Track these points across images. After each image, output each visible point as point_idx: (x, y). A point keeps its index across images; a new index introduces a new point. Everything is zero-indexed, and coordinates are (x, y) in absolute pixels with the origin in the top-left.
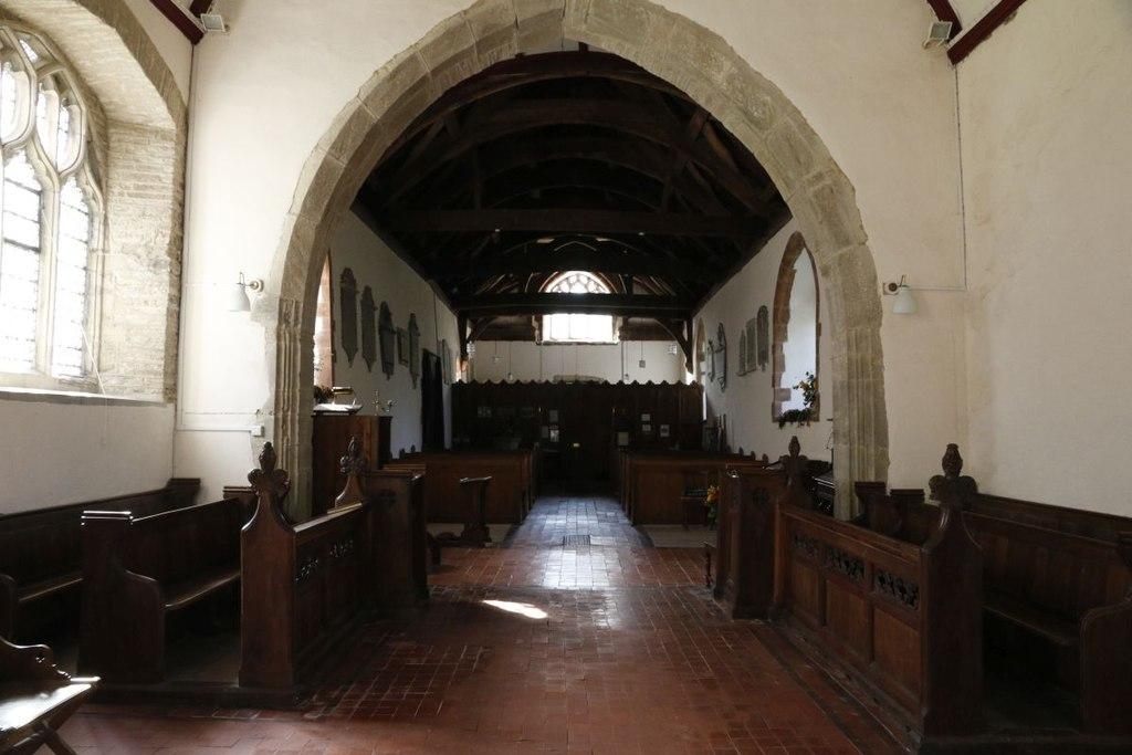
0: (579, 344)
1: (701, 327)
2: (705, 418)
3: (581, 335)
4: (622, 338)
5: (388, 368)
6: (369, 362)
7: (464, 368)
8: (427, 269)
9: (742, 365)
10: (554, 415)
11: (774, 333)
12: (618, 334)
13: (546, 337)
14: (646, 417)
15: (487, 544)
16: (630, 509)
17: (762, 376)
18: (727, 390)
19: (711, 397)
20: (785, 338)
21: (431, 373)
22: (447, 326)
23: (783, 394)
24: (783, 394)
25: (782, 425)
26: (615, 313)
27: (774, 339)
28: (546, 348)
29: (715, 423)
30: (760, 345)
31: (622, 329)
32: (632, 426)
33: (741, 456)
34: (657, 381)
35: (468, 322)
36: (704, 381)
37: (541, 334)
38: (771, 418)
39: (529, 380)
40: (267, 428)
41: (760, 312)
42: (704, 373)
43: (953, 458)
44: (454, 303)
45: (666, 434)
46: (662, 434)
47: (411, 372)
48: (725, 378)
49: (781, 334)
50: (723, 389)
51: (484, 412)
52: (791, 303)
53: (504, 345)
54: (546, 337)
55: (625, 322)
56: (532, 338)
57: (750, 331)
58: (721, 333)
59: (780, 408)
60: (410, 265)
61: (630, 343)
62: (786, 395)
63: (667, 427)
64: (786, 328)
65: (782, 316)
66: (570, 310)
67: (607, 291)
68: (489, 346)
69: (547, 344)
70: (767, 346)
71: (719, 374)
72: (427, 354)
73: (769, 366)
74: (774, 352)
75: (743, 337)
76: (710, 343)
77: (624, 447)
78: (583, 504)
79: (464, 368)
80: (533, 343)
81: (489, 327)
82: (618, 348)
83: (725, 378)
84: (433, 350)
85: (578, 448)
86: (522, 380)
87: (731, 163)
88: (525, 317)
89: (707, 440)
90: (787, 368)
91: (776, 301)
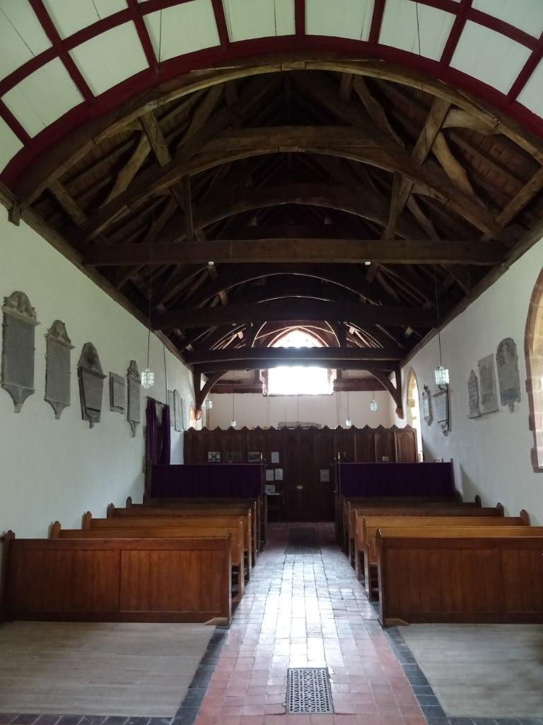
3: (299, 383)
5: (90, 413)
6: (57, 401)
8: (153, 320)
9: (475, 406)
10: (275, 457)
12: (332, 386)
16: (373, 584)
18: (450, 433)
19: (430, 442)
21: (157, 424)
22: (181, 381)
26: (330, 365)
28: (271, 398)
35: (202, 375)
39: (268, 427)
40: (475, 371)
41: (501, 345)
42: (415, 418)
43: (91, 426)
44: (187, 358)
47: (128, 419)
48: (448, 422)
53: (238, 397)
55: (339, 374)
57: (485, 370)
66: (291, 363)
67: (319, 345)
69: (271, 396)
71: (439, 416)
72: (151, 403)
73: (522, 405)
83: (448, 422)
85: (300, 484)
86: (262, 427)
87: (464, 183)
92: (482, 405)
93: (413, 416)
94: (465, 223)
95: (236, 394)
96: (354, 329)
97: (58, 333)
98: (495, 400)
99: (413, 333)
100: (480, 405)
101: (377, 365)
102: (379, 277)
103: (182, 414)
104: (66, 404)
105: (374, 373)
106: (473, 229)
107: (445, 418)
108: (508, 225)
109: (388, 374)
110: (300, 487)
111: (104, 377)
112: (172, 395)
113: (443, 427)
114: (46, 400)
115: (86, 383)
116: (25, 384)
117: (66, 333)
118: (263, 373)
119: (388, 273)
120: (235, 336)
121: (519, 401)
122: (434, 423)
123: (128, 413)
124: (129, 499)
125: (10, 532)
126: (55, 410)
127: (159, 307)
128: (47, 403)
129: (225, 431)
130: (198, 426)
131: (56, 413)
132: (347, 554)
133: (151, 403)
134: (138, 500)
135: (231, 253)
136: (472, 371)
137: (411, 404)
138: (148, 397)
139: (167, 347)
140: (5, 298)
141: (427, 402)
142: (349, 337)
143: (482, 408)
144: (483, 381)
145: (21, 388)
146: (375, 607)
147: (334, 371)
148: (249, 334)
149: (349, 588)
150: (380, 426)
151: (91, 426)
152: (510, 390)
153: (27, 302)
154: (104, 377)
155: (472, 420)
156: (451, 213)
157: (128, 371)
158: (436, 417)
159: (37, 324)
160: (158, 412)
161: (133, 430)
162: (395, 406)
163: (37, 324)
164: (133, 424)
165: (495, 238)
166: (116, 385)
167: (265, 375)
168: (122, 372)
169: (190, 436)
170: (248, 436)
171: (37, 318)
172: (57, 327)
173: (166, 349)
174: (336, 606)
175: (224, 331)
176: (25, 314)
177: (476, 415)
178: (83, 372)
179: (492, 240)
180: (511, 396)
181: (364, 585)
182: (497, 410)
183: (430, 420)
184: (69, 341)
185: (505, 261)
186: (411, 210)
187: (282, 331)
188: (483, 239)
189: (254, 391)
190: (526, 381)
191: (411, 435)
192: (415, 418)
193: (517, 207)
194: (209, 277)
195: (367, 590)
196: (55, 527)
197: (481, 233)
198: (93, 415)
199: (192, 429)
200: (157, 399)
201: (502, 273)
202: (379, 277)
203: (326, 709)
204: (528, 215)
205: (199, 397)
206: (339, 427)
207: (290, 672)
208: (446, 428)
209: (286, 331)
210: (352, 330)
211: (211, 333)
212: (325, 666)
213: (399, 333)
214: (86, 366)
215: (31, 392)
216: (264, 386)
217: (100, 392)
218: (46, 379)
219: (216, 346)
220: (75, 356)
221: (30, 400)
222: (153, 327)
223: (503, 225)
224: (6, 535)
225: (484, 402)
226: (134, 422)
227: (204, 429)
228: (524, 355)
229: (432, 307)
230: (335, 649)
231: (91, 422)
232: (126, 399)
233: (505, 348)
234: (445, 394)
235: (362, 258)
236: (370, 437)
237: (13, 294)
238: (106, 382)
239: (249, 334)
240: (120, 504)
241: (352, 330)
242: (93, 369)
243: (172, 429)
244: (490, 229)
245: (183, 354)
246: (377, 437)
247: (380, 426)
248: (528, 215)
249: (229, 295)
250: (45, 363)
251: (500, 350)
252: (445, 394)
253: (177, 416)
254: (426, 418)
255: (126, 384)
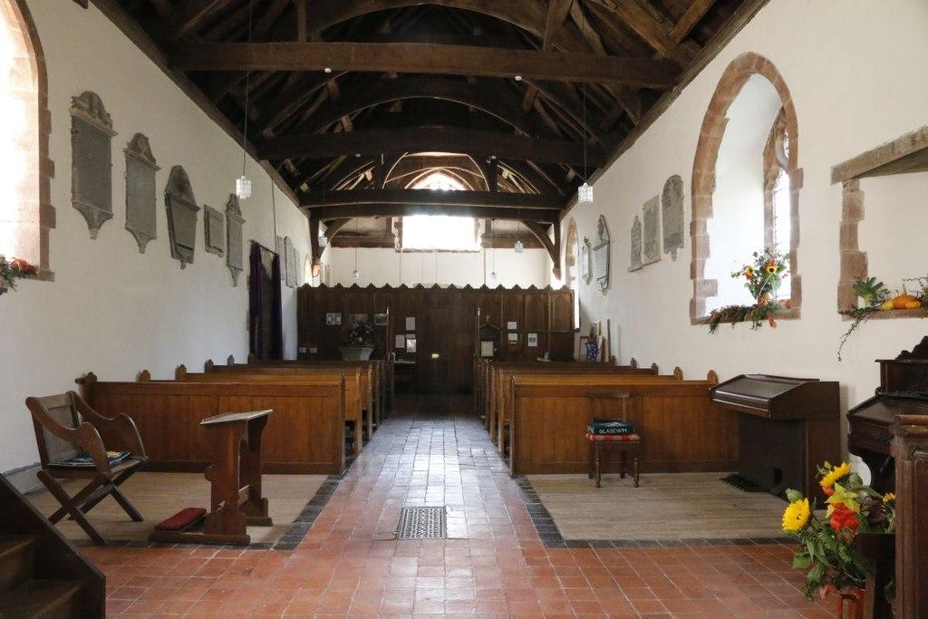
0: (440, 251)
1: (572, 228)
2: (577, 325)
3: (443, 245)
4: (485, 245)
5: (182, 251)
6: (141, 232)
7: (316, 272)
9: (636, 256)
10: (410, 323)
11: (694, 207)
12: (480, 240)
13: (406, 245)
14: (512, 325)
15: (255, 533)
16: (506, 443)
17: (672, 268)
18: (609, 291)
19: (586, 302)
20: (709, 213)
21: (264, 281)
22: (288, 225)
23: (707, 288)
24: (707, 288)
25: (713, 328)
26: (478, 213)
27: (694, 215)
29: (593, 330)
30: (674, 222)
31: (485, 236)
32: (496, 334)
33: (633, 370)
34: (525, 286)
36: (574, 286)
37: (400, 242)
38: (688, 320)
41: (668, 184)
42: (574, 278)
43: (183, 267)
44: (302, 200)
45: (535, 344)
46: (530, 344)
47: (228, 264)
48: (608, 278)
49: (702, 205)
50: (604, 291)
51: (334, 319)
52: (717, 165)
54: (406, 245)
55: (488, 227)
56: (391, 245)
57: (650, 215)
58: (603, 226)
59: (703, 306)
60: (220, 125)
61: (490, 251)
62: (712, 289)
63: (535, 336)
64: (711, 199)
65: (703, 181)
66: (432, 210)
68: (348, 253)
69: (407, 251)
70: (680, 227)
71: (599, 272)
72: (256, 249)
73: (685, 253)
74: (693, 232)
75: (637, 223)
76: (586, 241)
77: (489, 358)
78: (440, 432)
79: (316, 272)
80: (392, 250)
81: (340, 233)
82: (480, 256)
84: (267, 242)
88: (383, 220)
89: (580, 350)
90: (712, 254)
91: (697, 164)
92: (644, 256)
93: (572, 275)
94: (636, 38)
95: (360, 249)
96: (508, 172)
97: (139, 150)
98: (658, 249)
99: (576, 176)
100: (643, 255)
101: (537, 213)
102: (538, 104)
103: (295, 266)
104: (150, 235)
105: (529, 226)
106: (646, 45)
107: (605, 274)
108: (684, 40)
109: (547, 228)
110: (435, 356)
111: (197, 209)
112: (283, 243)
113: (602, 284)
114: (126, 228)
115: (174, 213)
116: (101, 206)
117: (149, 149)
118: (396, 223)
119: (547, 99)
120: (362, 177)
121: (682, 248)
122: (594, 281)
123: (228, 257)
124: (231, 358)
125: (91, 374)
126: (138, 241)
127: (265, 132)
128: (129, 233)
129: (347, 289)
130: (315, 283)
131: (139, 245)
132: (488, 429)
133: (256, 249)
134: (241, 358)
135: (353, 58)
136: (637, 217)
137: (570, 262)
138: (252, 241)
139: (276, 183)
140: (74, 98)
141: (586, 256)
142: (501, 183)
143: (643, 259)
144: (646, 227)
145: (96, 211)
146: (507, 463)
147: (482, 221)
148: (379, 174)
149: (481, 447)
150: (533, 287)
151: (183, 267)
152: (674, 235)
153: (100, 105)
154: (197, 209)
155: (633, 274)
156: (622, 26)
157: (227, 206)
158: (596, 275)
159: (115, 134)
160: (266, 261)
161: (234, 277)
162: (552, 264)
163: (115, 134)
164: (235, 271)
165: (668, 56)
166: (212, 221)
167: (399, 225)
168: (220, 207)
169: (305, 293)
170: (375, 295)
171: (114, 125)
172: (139, 142)
173: (276, 186)
174: (462, 462)
175: (351, 166)
176: (98, 120)
177: (637, 267)
178: (172, 201)
179: (664, 59)
180: (674, 241)
181: (497, 446)
182: (659, 260)
183: (589, 279)
184: (154, 160)
185: (676, 84)
186: (575, 19)
187: (422, 172)
188: (656, 58)
189: (384, 246)
190: (691, 224)
191: (567, 297)
192: (574, 278)
193: (694, 19)
194: (329, 97)
195: (500, 450)
196: (145, 375)
197: (653, 51)
198: (185, 253)
199: (307, 286)
200: (261, 243)
201: (673, 99)
202: (538, 104)
203: (439, 535)
204: (706, 30)
205: (316, 251)
206: (484, 286)
207: (404, 511)
208: (605, 286)
209: (422, 175)
210: (506, 173)
211: (331, 171)
212: (442, 505)
213: (558, 174)
214: (177, 194)
215: (110, 216)
216: (396, 240)
217: (193, 226)
218: (127, 204)
219: (340, 185)
220: (162, 181)
221: (106, 226)
222: (259, 156)
223: (678, 40)
224: (86, 377)
225: (647, 251)
226: (235, 268)
227: (322, 285)
228: (690, 192)
229: (597, 143)
230: (357, 221)
231: (182, 261)
232: (225, 239)
233: (671, 187)
234: (606, 247)
235: (511, 71)
236: (520, 298)
237: (83, 95)
238: (200, 215)
239: (379, 174)
240: (220, 361)
241: (506, 173)
242: (184, 197)
243: (283, 283)
244: (663, 45)
245: (296, 194)
246: (528, 298)
247: (533, 287)
248: (706, 30)
249: (355, 123)
250: (125, 184)
251: (666, 190)
252: (606, 247)
253: (289, 269)
254: (584, 276)
255: (225, 223)
